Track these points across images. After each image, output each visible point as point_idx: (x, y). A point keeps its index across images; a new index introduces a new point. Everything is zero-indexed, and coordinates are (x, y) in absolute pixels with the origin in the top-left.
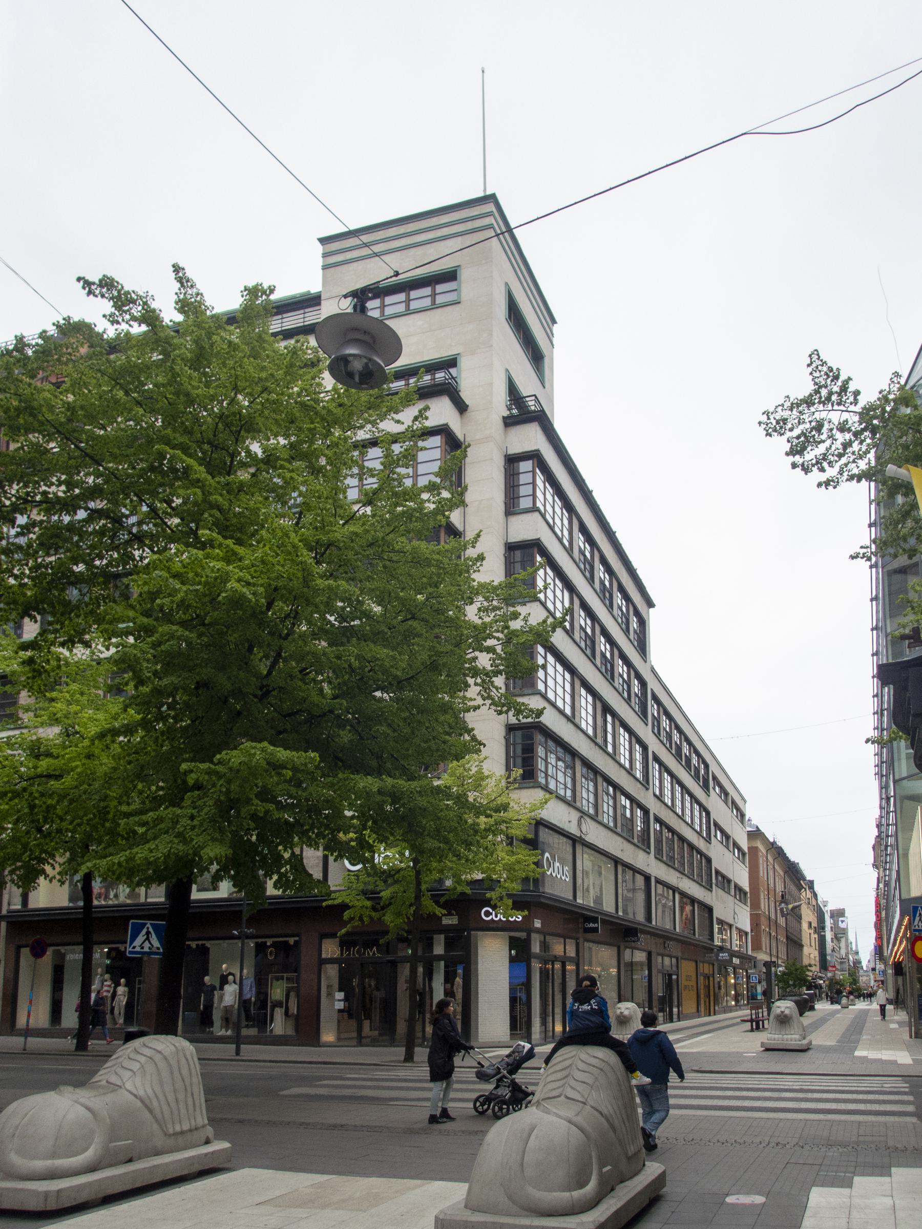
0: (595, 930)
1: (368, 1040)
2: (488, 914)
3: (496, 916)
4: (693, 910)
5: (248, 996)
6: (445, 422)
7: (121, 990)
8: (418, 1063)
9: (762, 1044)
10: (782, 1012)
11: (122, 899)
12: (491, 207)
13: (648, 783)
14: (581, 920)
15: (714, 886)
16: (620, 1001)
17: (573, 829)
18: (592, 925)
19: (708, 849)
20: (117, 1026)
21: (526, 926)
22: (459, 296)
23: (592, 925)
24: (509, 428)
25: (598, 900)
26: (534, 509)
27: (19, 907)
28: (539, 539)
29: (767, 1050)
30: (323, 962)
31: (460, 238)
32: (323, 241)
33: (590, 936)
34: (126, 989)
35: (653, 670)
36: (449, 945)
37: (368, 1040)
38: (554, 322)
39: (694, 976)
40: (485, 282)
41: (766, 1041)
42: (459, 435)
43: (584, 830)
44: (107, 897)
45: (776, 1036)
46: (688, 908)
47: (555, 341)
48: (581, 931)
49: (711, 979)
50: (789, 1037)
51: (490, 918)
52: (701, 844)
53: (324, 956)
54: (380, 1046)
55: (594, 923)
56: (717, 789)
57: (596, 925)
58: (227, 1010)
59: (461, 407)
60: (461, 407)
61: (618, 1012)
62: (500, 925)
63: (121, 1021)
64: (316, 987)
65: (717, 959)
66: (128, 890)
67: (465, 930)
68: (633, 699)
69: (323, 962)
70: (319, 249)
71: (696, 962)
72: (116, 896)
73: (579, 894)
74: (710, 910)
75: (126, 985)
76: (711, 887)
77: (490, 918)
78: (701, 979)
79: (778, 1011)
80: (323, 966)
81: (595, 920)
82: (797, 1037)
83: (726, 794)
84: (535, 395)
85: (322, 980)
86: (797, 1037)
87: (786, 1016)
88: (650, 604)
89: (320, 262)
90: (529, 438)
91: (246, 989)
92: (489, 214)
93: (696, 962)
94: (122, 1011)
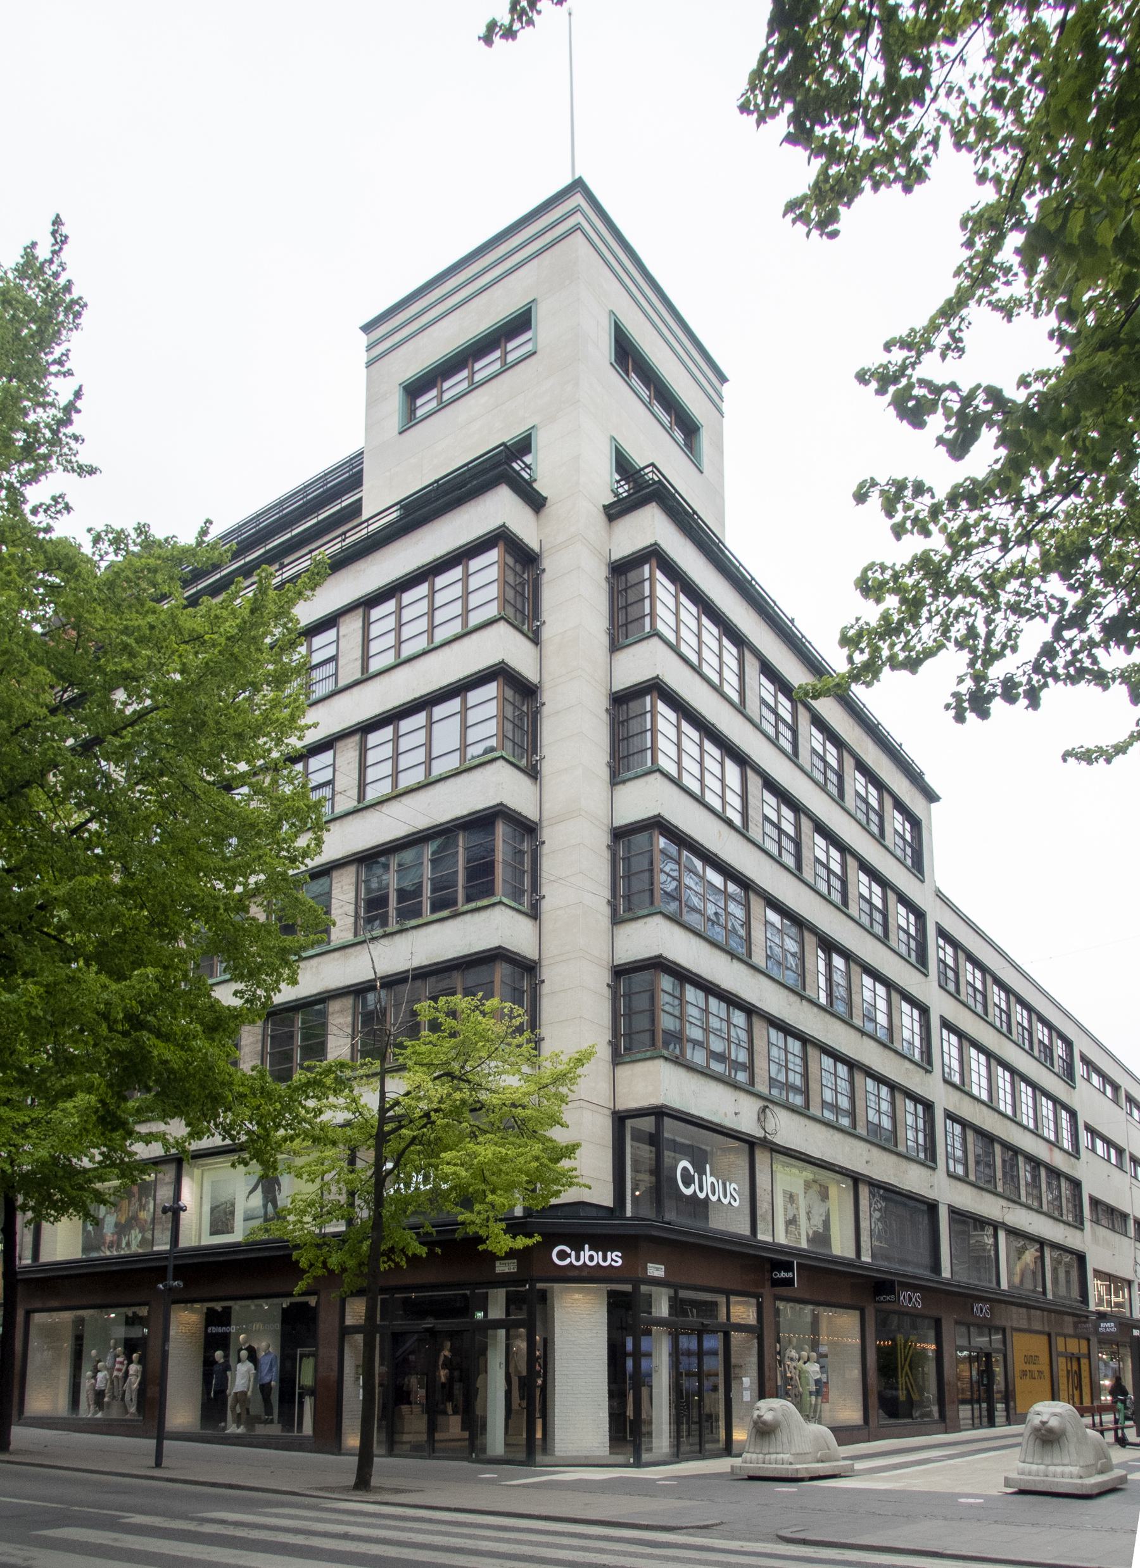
0: (789, 1282)
1: (407, 1447)
2: (563, 1255)
3: (578, 1259)
4: (1042, 1257)
5: (267, 1380)
6: (500, 523)
7: (133, 1368)
8: (380, 1489)
9: (1008, 1482)
10: (1044, 1423)
11: (135, 1248)
12: (578, 199)
13: (930, 1063)
14: (768, 1266)
15: (1087, 1224)
16: (762, 1395)
17: (748, 1124)
18: (783, 1275)
19: (1073, 1167)
20: (128, 1417)
21: (631, 1274)
22: (536, 345)
23: (783, 1275)
24: (615, 523)
25: (822, 1238)
26: (655, 634)
27: (29, 1262)
28: (657, 677)
29: (1022, 1492)
30: (345, 1331)
31: (535, 261)
32: (367, 328)
33: (780, 1290)
34: (139, 1367)
35: (939, 895)
36: (512, 1301)
37: (407, 1447)
38: (723, 379)
39: (1044, 1359)
40: (578, 311)
41: (1014, 1475)
42: (532, 542)
43: (770, 1127)
44: (119, 1246)
45: (1034, 1467)
46: (1030, 1255)
47: (725, 407)
48: (768, 1284)
49: (1084, 1361)
50: (1059, 1469)
51: (568, 1261)
52: (1059, 1161)
53: (349, 1321)
54: (438, 1458)
55: (787, 1271)
56: (1095, 1079)
57: (790, 1275)
58: (241, 1397)
59: (536, 502)
60: (536, 502)
61: (756, 1413)
62: (585, 1274)
63: (133, 1410)
64: (335, 1367)
65: (1096, 1332)
66: (140, 1236)
67: (526, 1281)
68: (892, 936)
69: (345, 1331)
70: (363, 339)
71: (1049, 1335)
72: (128, 1244)
73: (760, 1226)
74: (1081, 1258)
75: (139, 1362)
76: (1082, 1223)
77: (568, 1261)
78: (1062, 1364)
79: (1036, 1421)
80: (347, 1338)
81: (788, 1267)
82: (1075, 1470)
83: (1116, 1088)
84: (652, 465)
85: (346, 1357)
86: (1075, 1470)
87: (1051, 1431)
88: (931, 796)
89: (364, 357)
90: (650, 527)
91: (265, 1368)
92: (577, 209)
93: (1049, 1335)
94: (134, 1397)
